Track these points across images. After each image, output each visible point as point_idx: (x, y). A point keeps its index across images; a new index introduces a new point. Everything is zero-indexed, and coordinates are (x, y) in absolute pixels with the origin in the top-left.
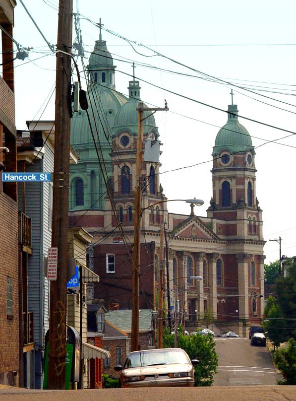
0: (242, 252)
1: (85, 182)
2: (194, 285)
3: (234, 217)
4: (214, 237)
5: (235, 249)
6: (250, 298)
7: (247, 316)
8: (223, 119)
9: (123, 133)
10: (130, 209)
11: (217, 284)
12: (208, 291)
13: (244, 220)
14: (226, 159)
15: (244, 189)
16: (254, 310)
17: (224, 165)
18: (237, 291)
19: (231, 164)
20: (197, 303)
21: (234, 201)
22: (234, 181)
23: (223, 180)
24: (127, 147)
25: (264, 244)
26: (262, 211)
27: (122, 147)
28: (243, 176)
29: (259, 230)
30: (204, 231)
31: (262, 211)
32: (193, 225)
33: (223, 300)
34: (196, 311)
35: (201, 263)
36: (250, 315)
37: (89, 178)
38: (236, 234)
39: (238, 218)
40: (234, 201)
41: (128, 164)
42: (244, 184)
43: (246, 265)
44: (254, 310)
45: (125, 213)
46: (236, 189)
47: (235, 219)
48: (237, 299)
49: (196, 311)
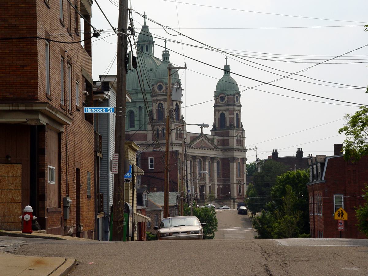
0: (233, 156)
1: (135, 113)
2: (203, 176)
3: (227, 135)
4: (215, 147)
5: (228, 154)
6: (237, 185)
7: (236, 196)
8: (221, 74)
9: (221, 94)
10: (163, 129)
11: (217, 176)
12: (211, 180)
13: (234, 136)
14: (222, 99)
15: (234, 118)
16: (240, 192)
17: (221, 102)
18: (229, 181)
19: (225, 102)
20: (205, 188)
21: (228, 125)
22: (228, 112)
23: (221, 112)
24: (161, 91)
25: (246, 151)
26: (245, 131)
27: (159, 91)
28: (233, 109)
29: (243, 142)
30: (209, 143)
31: (245, 131)
32: (202, 140)
33: (221, 186)
34: (204, 193)
35: (207, 163)
36: (238, 195)
37: (138, 110)
38: (229, 145)
39: (230, 136)
40: (228, 125)
41: (162, 102)
42: (233, 114)
43: (235, 164)
44: (240, 192)
45: (160, 132)
46: (229, 117)
47: (228, 136)
48: (229, 185)
49: (204, 193)
